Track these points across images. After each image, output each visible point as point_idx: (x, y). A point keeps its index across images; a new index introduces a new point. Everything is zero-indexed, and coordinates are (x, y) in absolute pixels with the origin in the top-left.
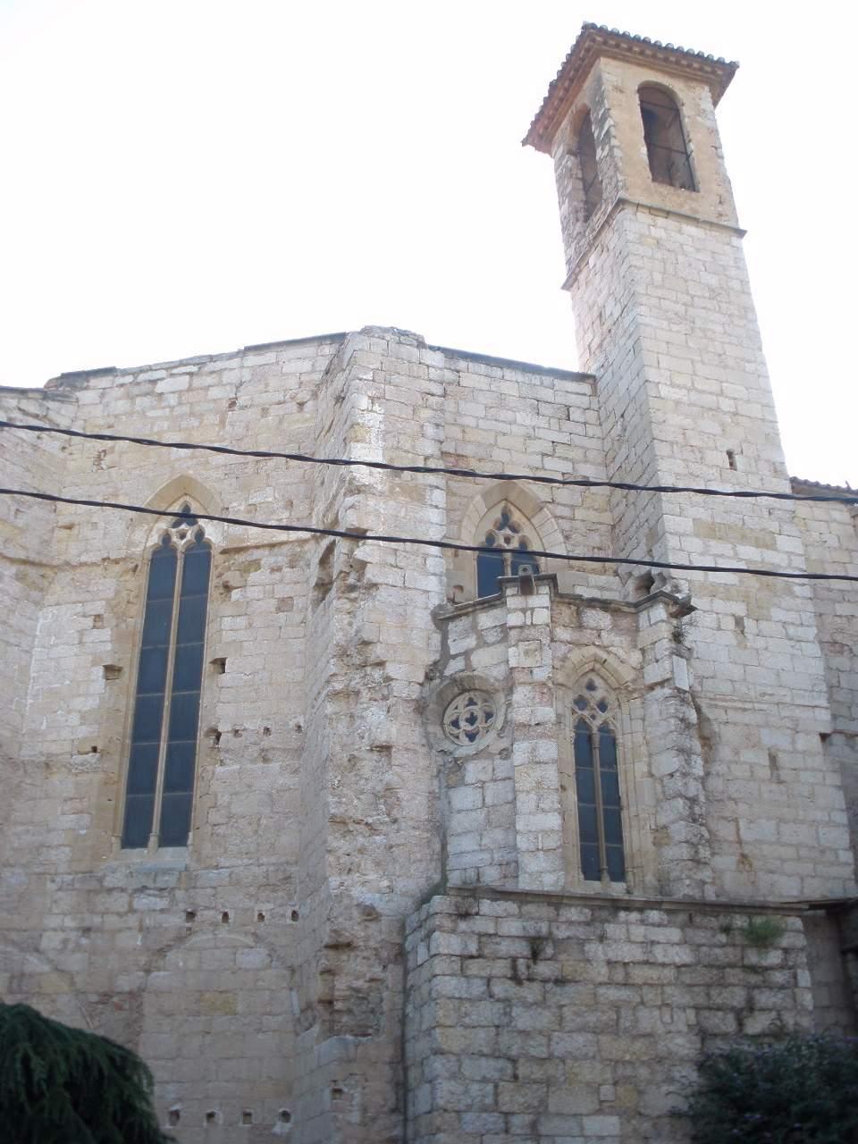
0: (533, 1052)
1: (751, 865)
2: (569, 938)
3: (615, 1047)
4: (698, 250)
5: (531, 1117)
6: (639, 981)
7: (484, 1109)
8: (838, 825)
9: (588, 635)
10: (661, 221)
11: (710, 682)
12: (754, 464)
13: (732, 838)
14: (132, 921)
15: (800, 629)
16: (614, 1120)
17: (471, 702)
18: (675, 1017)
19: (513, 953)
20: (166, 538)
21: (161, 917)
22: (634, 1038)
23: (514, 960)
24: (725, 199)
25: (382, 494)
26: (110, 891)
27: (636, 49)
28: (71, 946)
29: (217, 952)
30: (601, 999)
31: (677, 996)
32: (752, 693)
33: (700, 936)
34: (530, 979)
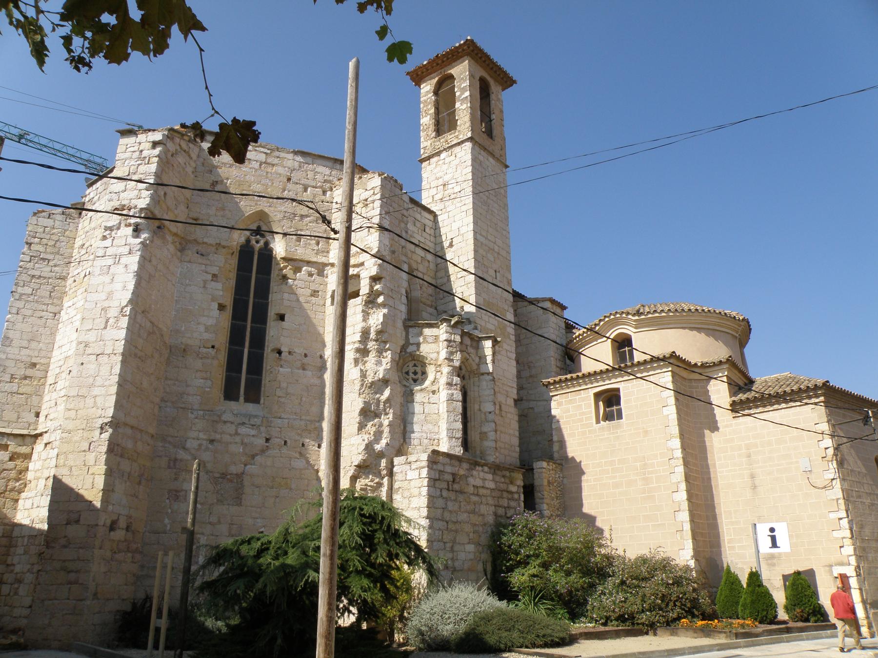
3: (475, 519)
14: (238, 439)
17: (415, 365)
20: (248, 241)
21: (252, 439)
24: (503, 148)
26: (225, 422)
28: (203, 448)
33: (498, 478)
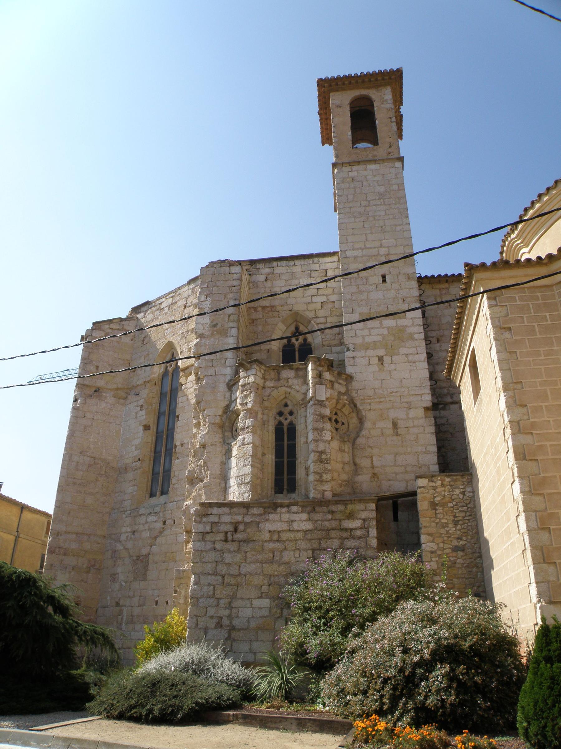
0: (231, 572)
1: (378, 478)
2: (252, 521)
3: (269, 569)
4: (375, 176)
5: (229, 600)
6: (284, 539)
7: (209, 597)
8: (430, 453)
9: (282, 382)
10: (355, 168)
11: (362, 391)
12: (396, 278)
13: (370, 465)
14: (146, 527)
15: (416, 356)
16: (268, 600)
18: (301, 554)
19: (226, 530)
22: (280, 565)
23: (226, 533)
25: (208, 336)
26: (141, 515)
27: (366, 80)
29: (171, 536)
30: (265, 548)
31: (303, 545)
32: (386, 393)
34: (233, 541)
